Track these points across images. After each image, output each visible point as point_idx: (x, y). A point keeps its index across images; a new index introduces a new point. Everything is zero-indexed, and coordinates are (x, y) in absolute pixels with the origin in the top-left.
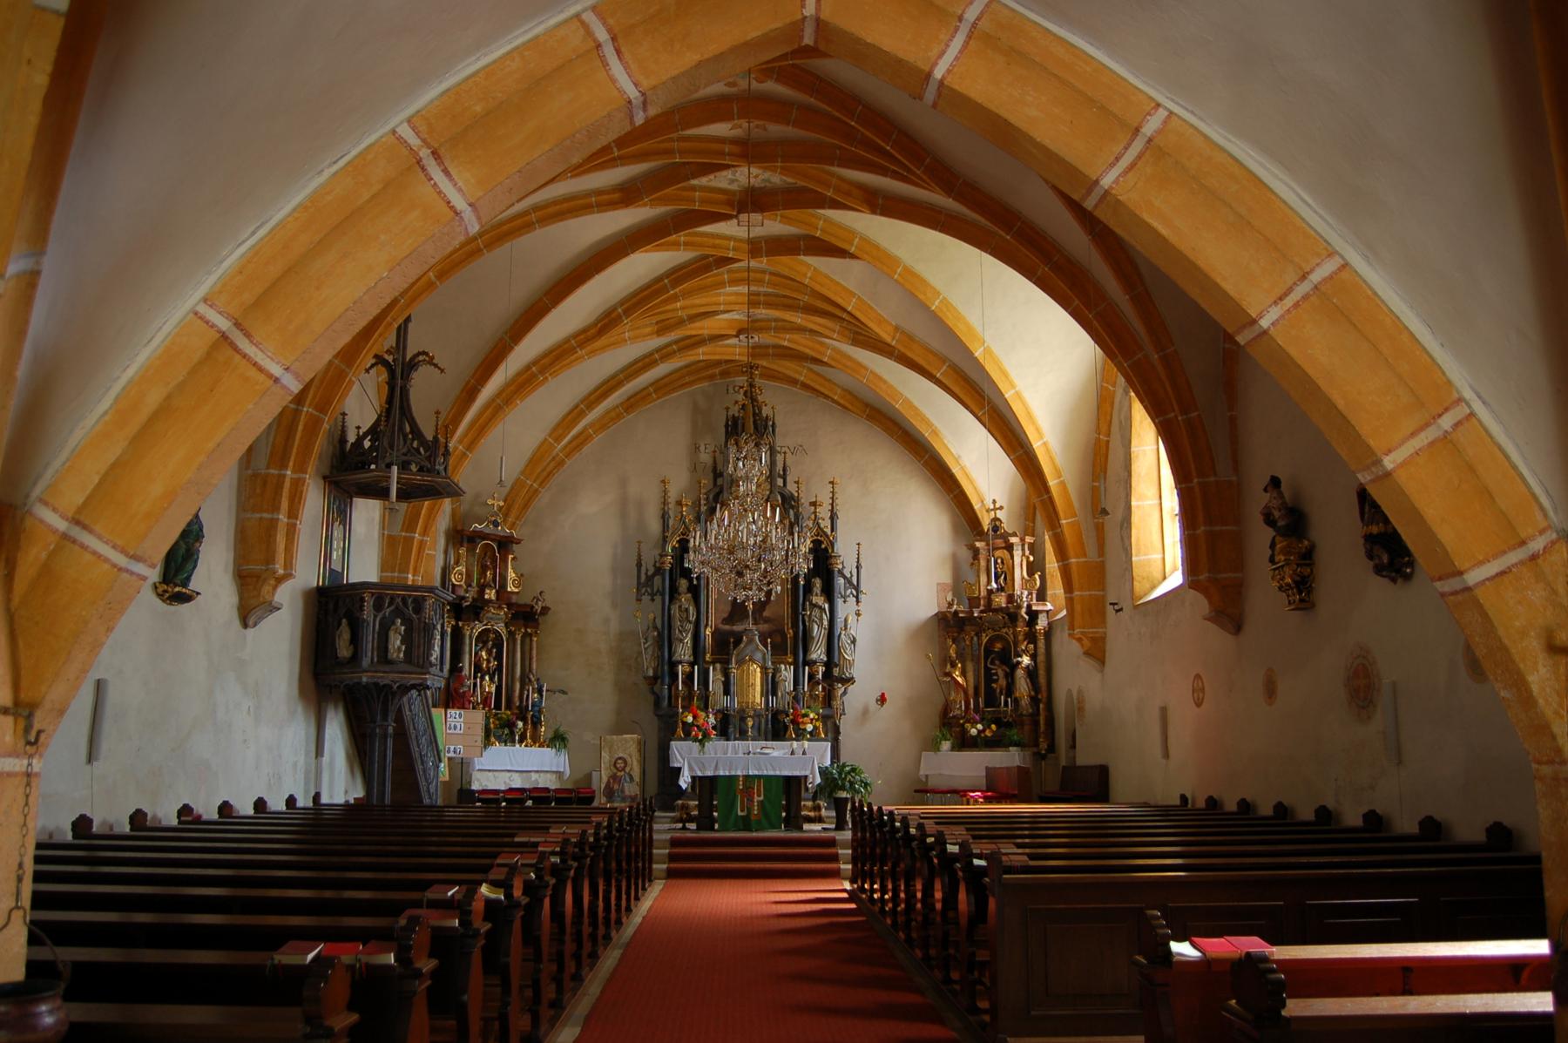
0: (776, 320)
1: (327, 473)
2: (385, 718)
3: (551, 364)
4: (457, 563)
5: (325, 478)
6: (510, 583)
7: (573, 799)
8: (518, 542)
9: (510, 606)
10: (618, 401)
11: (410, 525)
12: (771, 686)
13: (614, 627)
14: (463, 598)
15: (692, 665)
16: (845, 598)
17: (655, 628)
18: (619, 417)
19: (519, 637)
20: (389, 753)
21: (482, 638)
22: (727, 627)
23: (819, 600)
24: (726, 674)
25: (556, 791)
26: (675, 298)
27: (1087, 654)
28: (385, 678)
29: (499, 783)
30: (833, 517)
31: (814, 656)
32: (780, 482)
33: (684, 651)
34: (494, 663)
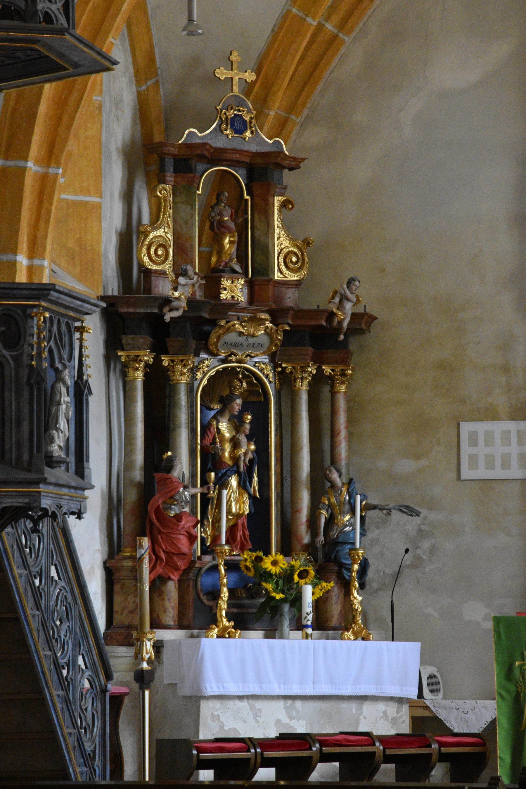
4: (155, 222)
6: (278, 261)
8: (294, 164)
9: (276, 316)
14: (167, 301)
21: (218, 392)
25: (385, 740)
29: (265, 724)
34: (248, 449)
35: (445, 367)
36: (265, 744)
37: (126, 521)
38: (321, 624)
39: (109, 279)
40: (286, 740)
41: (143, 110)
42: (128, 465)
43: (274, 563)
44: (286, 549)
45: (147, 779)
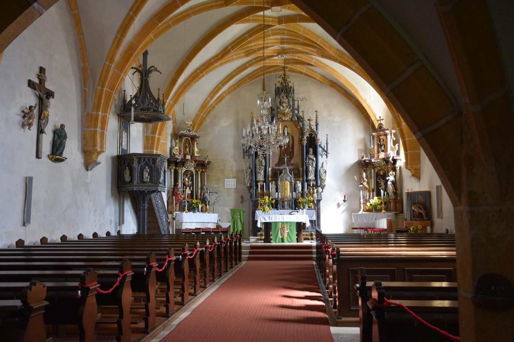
0: (292, 49)
1: (119, 113)
2: (144, 203)
3: (205, 69)
4: (176, 146)
5: (118, 115)
6: (195, 153)
7: (218, 230)
9: (195, 161)
10: (234, 83)
11: (154, 132)
12: (294, 189)
13: (235, 168)
14: (178, 159)
15: (264, 182)
16: (322, 155)
17: (250, 168)
18: (235, 89)
19: (199, 173)
20: (146, 216)
22: (277, 168)
23: (312, 156)
24: (277, 185)
25: (212, 229)
26: (251, 42)
27: (413, 175)
28: (143, 189)
29: (193, 226)
30: (317, 125)
31: (310, 178)
32: (296, 112)
33: (261, 177)
34: (190, 183)
35: (222, 170)
36: (193, 230)
37: (170, 194)
38: (202, 211)
39: (168, 155)
40: (196, 229)
41: (174, 128)
42: (171, 185)
43: (195, 201)
44: (196, 199)
45: (117, 307)
